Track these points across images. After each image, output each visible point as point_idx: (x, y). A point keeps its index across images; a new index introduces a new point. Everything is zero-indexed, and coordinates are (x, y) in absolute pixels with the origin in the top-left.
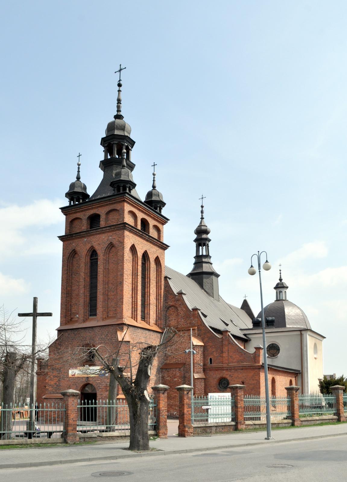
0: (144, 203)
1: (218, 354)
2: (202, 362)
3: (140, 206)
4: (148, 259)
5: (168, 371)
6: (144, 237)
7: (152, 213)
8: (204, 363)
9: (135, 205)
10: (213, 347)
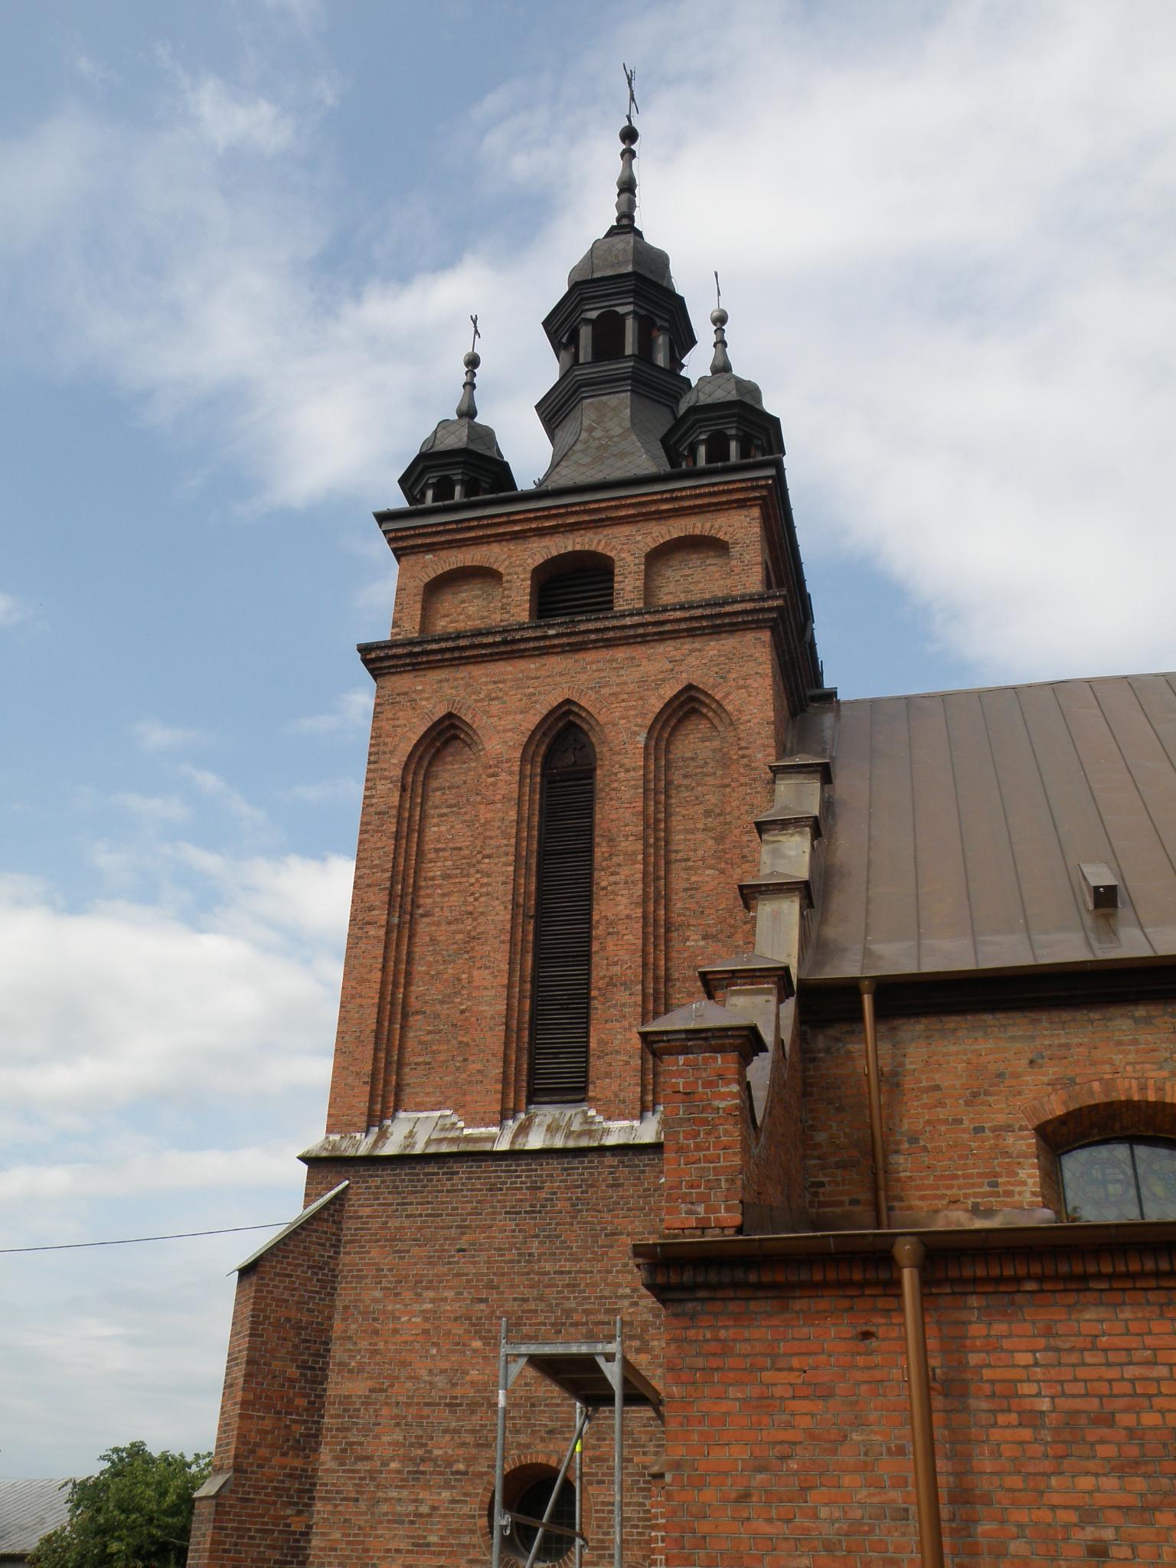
0: (465, 500)
4: (714, 630)
6: (531, 645)
7: (659, 497)
9: (472, 534)
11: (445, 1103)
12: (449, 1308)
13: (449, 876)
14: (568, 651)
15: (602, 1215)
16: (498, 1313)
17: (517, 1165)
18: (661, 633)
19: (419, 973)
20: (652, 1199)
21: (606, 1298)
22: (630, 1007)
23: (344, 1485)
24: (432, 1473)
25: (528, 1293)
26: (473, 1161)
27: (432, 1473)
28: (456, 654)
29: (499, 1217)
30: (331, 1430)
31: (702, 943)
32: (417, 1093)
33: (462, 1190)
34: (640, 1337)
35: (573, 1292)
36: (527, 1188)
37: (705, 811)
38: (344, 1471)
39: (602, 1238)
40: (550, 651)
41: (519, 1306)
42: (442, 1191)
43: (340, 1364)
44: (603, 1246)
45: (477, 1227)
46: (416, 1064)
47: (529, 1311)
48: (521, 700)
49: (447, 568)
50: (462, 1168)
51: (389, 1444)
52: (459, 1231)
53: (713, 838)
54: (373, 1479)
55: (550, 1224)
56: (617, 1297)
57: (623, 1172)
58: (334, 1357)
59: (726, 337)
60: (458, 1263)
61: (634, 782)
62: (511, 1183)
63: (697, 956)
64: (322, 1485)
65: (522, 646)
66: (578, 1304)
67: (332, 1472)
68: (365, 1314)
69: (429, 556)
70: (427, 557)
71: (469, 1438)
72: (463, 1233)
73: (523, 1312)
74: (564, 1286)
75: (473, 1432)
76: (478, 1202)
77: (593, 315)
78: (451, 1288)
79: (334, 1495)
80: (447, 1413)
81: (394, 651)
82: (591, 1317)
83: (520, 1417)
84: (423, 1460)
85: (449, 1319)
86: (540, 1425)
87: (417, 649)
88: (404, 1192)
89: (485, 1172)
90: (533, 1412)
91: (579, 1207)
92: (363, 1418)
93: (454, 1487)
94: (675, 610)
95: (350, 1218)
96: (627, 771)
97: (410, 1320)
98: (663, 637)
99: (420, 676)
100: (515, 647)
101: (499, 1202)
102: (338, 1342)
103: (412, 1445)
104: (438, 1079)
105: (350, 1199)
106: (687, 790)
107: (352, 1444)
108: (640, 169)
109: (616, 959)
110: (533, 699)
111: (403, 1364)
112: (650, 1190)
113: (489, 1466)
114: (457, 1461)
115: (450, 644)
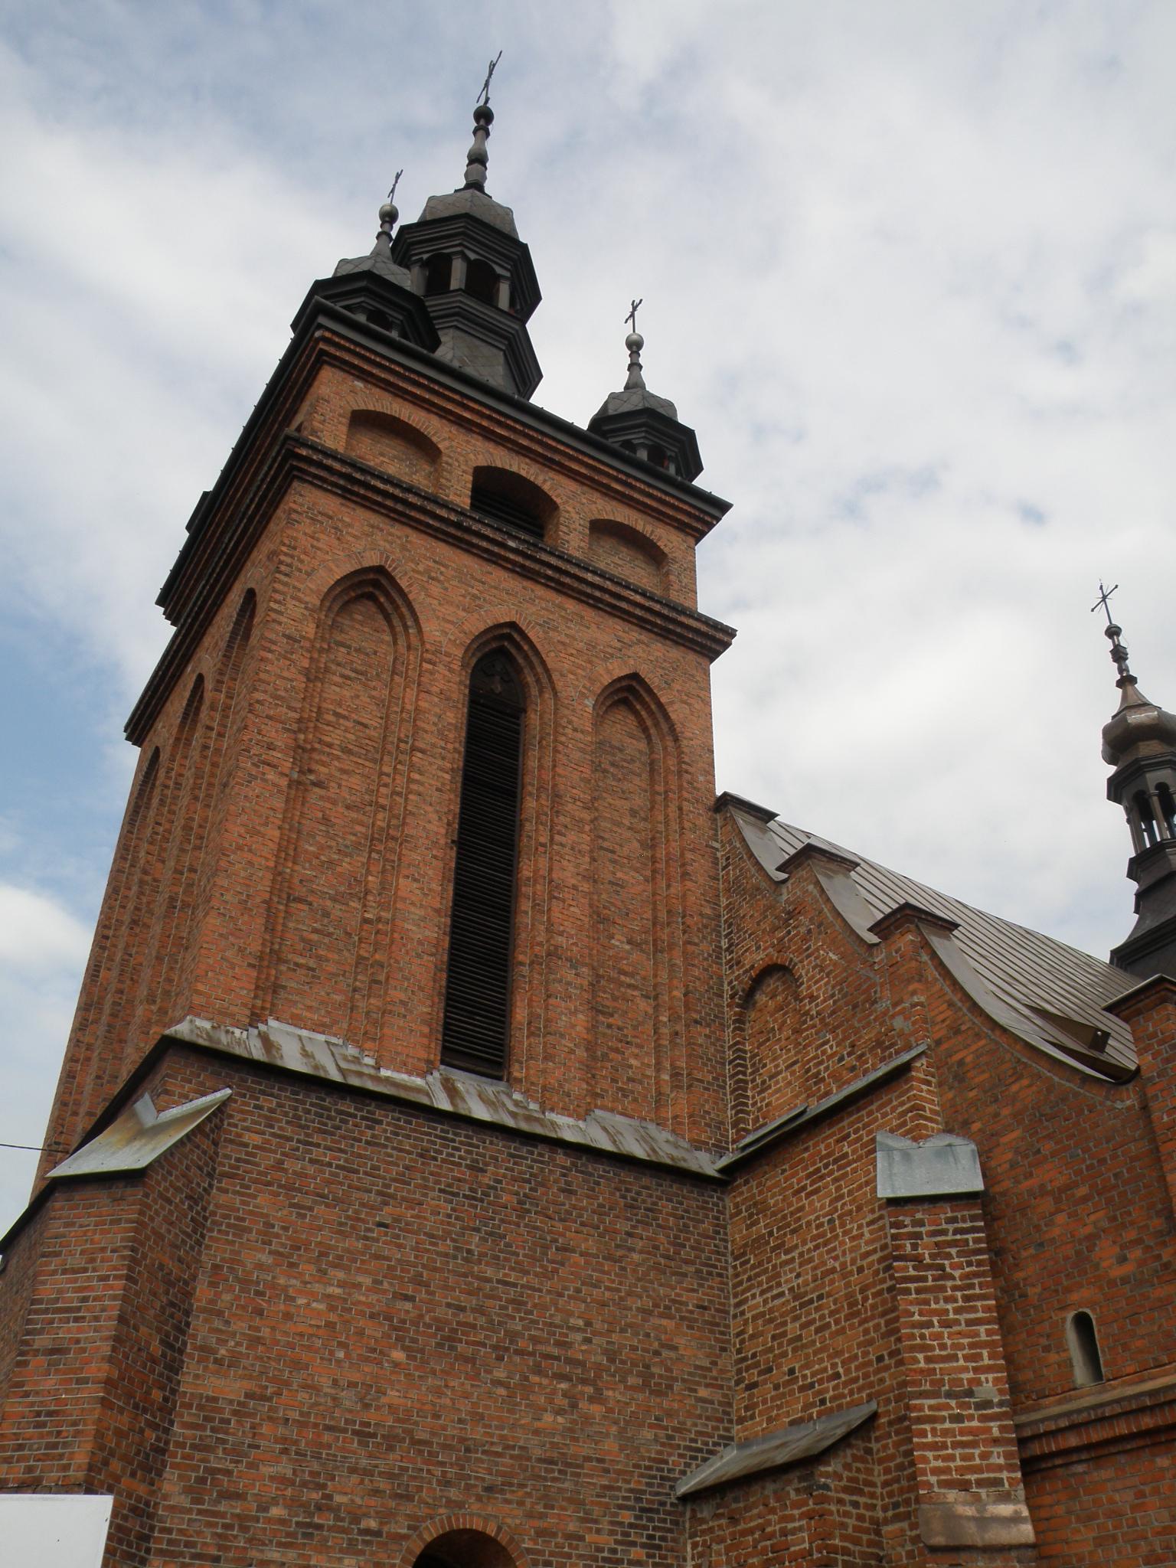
1: (1137, 1253)
2: (988, 1369)
3: (457, 397)
5: (733, 1520)
6: (484, 544)
8: (1011, 1380)
10: (1083, 1191)
11: (330, 1027)
12: (363, 1299)
13: (349, 752)
14: (517, 573)
15: (553, 1223)
16: (427, 1319)
17: (455, 1134)
18: (614, 607)
19: (306, 851)
20: (607, 1219)
21: (556, 1326)
22: (576, 988)
23: (199, 1533)
24: (330, 1529)
25: (465, 1300)
26: (400, 1112)
27: (330, 1529)
28: (400, 507)
29: (431, 1194)
30: (182, 1445)
31: (627, 947)
32: (295, 1003)
33: (386, 1147)
34: (592, 1382)
35: (518, 1311)
36: (467, 1166)
37: (631, 810)
38: (200, 1512)
39: (552, 1253)
40: (500, 562)
41: (454, 1315)
42: (360, 1141)
43: (202, 1348)
44: (553, 1262)
45: (403, 1199)
46: (296, 964)
47: (465, 1324)
48: (464, 596)
49: (379, 409)
50: (388, 1119)
51: (272, 1478)
52: (379, 1199)
53: (638, 841)
54: (244, 1529)
55: (493, 1219)
56: (569, 1328)
57: (575, 1177)
58: (194, 1337)
59: (641, 361)
60: (377, 1241)
61: (582, 746)
62: (448, 1155)
63: (622, 958)
64: (163, 1530)
65: (475, 541)
66: (525, 1328)
67: (181, 1512)
68: (245, 1282)
69: (359, 384)
70: (356, 383)
71: (382, 1484)
72: (386, 1204)
73: (458, 1323)
74: (509, 1301)
75: (390, 1476)
76: (407, 1168)
77: (472, 256)
78: (367, 1272)
79: (182, 1548)
80: (355, 1445)
81: (329, 462)
82: (539, 1347)
83: (452, 1465)
84: (319, 1508)
85: (362, 1313)
86: (477, 1478)
87: (358, 476)
88: (308, 1127)
89: (415, 1131)
90: (468, 1460)
91: (527, 1206)
92: (233, 1434)
93: (362, 1553)
94: (636, 592)
95: (231, 1142)
96: (575, 730)
97: (308, 1304)
98: (615, 612)
99: (348, 507)
100: (466, 537)
101: (431, 1174)
102: (202, 1316)
103: (304, 1484)
104: (323, 993)
105: (231, 1116)
106: (614, 780)
107: (213, 1471)
108: (491, 146)
109: (562, 928)
110: (477, 602)
111: (297, 1365)
112: (604, 1206)
113: (409, 1528)
114: (367, 1515)
115: (397, 492)
